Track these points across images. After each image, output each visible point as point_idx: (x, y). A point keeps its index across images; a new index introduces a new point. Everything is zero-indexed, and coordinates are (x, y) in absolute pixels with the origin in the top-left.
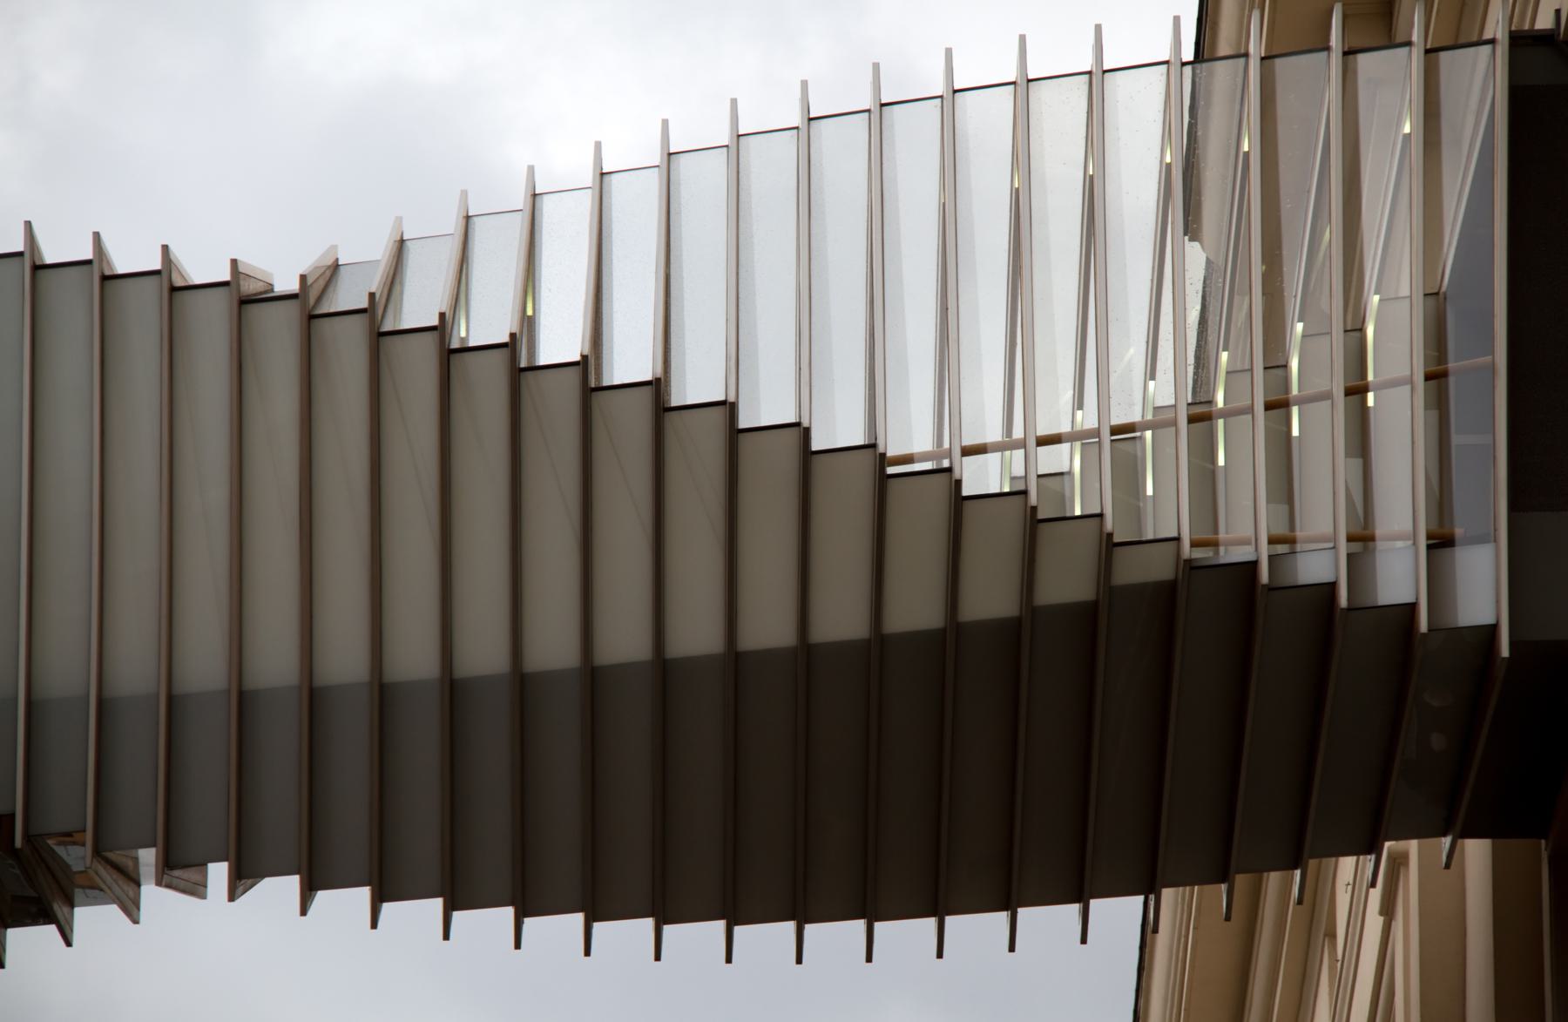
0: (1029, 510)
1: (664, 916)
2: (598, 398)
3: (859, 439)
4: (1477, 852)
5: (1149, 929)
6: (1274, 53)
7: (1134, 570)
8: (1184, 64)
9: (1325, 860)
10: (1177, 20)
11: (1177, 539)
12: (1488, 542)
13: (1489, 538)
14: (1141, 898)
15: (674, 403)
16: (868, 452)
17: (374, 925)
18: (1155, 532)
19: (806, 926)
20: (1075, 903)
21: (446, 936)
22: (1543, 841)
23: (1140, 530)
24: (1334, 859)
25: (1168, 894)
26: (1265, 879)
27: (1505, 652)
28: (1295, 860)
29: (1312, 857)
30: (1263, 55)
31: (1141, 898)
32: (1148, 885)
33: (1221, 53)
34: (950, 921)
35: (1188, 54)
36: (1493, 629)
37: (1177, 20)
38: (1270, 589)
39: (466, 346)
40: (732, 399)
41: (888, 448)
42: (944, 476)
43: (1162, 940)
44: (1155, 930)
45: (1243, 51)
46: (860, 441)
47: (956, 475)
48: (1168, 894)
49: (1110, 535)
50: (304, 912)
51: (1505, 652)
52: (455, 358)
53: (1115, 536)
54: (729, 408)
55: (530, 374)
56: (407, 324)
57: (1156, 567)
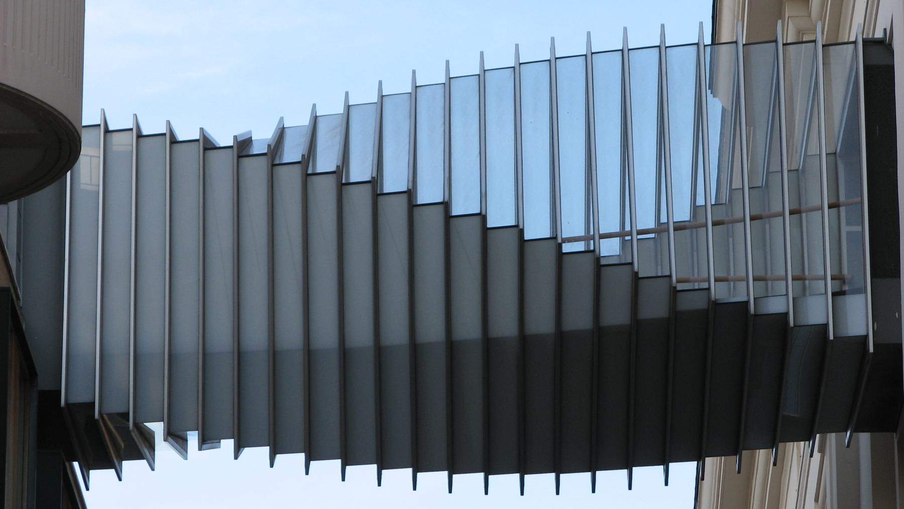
0: (672, 289)
1: (453, 470)
2: (381, 198)
3: (513, 223)
4: (864, 438)
5: (700, 478)
6: (750, 42)
7: (688, 303)
8: (705, 46)
9: (788, 443)
10: (701, 24)
11: (670, 276)
12: (862, 293)
13: (862, 290)
14: (696, 462)
15: (419, 203)
16: (553, 241)
17: (307, 473)
18: (662, 271)
19: (525, 476)
20: (868, 432)
21: (343, 479)
22: (895, 434)
23: (657, 273)
24: (758, 450)
25: (709, 461)
26: (787, 446)
27: (871, 350)
28: (735, 450)
29: (780, 442)
30: (744, 43)
31: (696, 462)
32: (699, 456)
33: (723, 41)
34: (599, 474)
35: (708, 40)
36: (866, 337)
37: (701, 24)
38: (756, 315)
39: (314, 172)
40: (446, 199)
41: (639, 270)
42: (590, 255)
43: (706, 484)
44: (703, 479)
45: (734, 40)
46: (513, 224)
47: (521, 227)
48: (709, 461)
49: (675, 288)
50: (272, 465)
51: (871, 350)
52: (309, 178)
53: (677, 287)
54: (482, 217)
55: (314, 177)
56: (286, 160)
57: (697, 303)
